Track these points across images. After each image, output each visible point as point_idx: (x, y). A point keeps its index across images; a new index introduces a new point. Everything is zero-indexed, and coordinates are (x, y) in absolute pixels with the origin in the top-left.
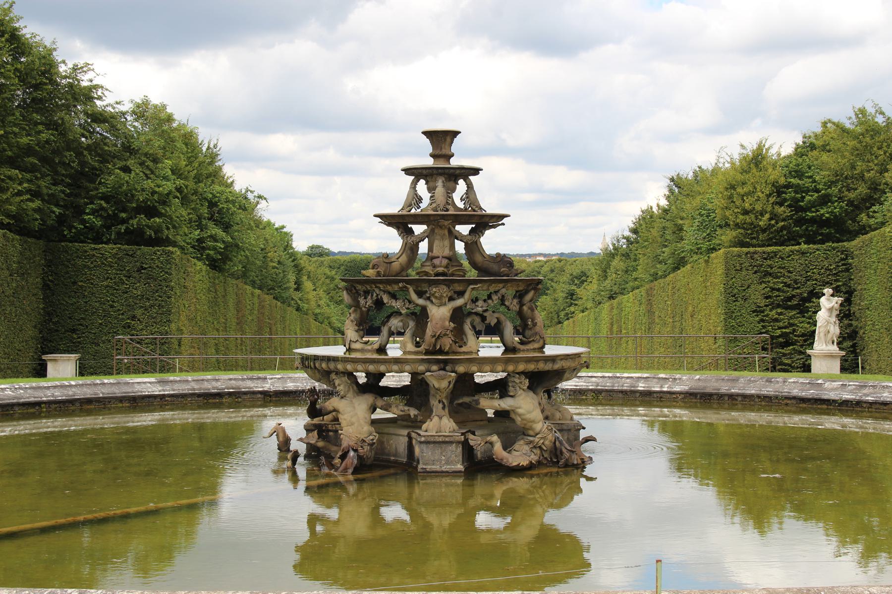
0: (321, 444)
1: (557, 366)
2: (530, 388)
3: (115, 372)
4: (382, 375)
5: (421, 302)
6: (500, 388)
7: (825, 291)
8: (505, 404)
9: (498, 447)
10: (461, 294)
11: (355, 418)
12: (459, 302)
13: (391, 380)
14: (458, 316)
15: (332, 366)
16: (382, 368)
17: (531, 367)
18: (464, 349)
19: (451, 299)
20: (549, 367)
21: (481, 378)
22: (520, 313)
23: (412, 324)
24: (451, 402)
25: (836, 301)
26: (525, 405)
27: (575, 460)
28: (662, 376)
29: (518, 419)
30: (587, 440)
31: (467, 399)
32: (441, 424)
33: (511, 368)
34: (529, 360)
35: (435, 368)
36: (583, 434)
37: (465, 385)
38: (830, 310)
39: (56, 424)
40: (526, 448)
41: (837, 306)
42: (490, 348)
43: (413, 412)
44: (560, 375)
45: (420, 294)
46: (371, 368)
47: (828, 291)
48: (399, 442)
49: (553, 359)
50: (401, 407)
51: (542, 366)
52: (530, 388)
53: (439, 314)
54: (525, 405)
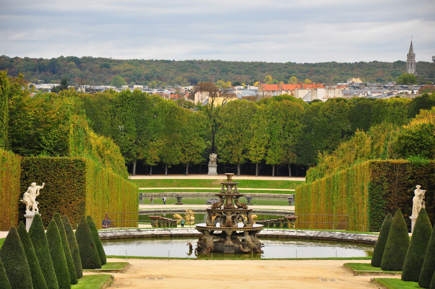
0: (201, 247)
5: (225, 215)
6: (242, 234)
7: (417, 186)
8: (243, 238)
9: (242, 247)
10: (234, 213)
11: (210, 241)
12: (233, 215)
14: (233, 218)
15: (205, 229)
17: (249, 230)
18: (234, 226)
19: (231, 214)
20: (253, 230)
21: (238, 232)
23: (222, 219)
24: (231, 237)
25: (423, 192)
26: (248, 238)
27: (258, 251)
31: (235, 237)
32: (229, 242)
33: (244, 230)
37: (234, 233)
38: (420, 196)
39: (288, 232)
40: (248, 248)
41: (423, 194)
43: (223, 239)
45: (224, 213)
46: (211, 230)
47: (418, 186)
48: (220, 246)
49: (254, 228)
53: (229, 217)
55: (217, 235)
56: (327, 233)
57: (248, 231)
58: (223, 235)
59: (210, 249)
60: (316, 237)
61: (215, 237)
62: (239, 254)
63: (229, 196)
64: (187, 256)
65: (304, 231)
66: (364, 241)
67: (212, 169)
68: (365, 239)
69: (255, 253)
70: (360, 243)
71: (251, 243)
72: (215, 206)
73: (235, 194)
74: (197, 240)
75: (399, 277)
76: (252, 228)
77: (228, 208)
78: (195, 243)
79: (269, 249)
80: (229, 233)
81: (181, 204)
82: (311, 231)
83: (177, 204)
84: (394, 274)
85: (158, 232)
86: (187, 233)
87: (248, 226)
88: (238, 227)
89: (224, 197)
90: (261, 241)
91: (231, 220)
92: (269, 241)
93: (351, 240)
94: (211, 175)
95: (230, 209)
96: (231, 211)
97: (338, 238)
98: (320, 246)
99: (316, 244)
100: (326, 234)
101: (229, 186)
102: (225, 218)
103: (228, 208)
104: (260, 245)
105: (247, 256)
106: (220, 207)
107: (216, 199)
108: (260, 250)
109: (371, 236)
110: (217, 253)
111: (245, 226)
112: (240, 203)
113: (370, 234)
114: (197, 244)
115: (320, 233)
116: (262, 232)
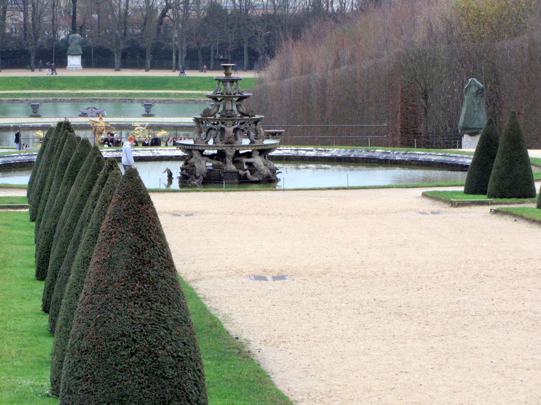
1: (268, 147)
2: (260, 155)
3: (117, 60)
4: (204, 150)
6: (249, 155)
13: (208, 152)
14: (235, 130)
15: (193, 148)
16: (204, 148)
17: (260, 148)
18: (237, 142)
19: (233, 125)
20: (266, 148)
22: (255, 129)
23: (219, 133)
26: (258, 160)
27: (273, 178)
28: (320, 149)
29: (255, 166)
30: (278, 173)
31: (239, 159)
33: (253, 148)
34: (258, 146)
35: (229, 148)
36: (277, 171)
37: (237, 154)
39: (304, 152)
42: (246, 142)
43: (221, 163)
44: (270, 150)
49: (267, 145)
50: (229, 165)
51: (263, 148)
52: (260, 155)
53: (230, 130)
54: (258, 160)
55: (211, 157)
56: (364, 151)
57: (259, 150)
58: (221, 156)
59: (201, 178)
60: (347, 158)
61: (209, 160)
62: (243, 182)
63: (227, 97)
64: (163, 187)
65: (327, 149)
66: (420, 161)
67: (74, 61)
68: (421, 158)
69: (269, 181)
70: (415, 165)
71: (263, 167)
72: (207, 113)
73: (237, 95)
74: (181, 164)
75: (534, 206)
76: (262, 146)
77: (228, 116)
78: (176, 168)
79: (287, 175)
80: (230, 153)
81: (39, 116)
82: (338, 149)
83: (32, 116)
84: (523, 202)
85: (108, 154)
86: (151, 155)
87: (258, 142)
88: (243, 144)
89: (219, 99)
90: (277, 165)
91: (232, 134)
92: (287, 166)
93: (400, 160)
94: (72, 70)
95: (230, 117)
96: (232, 120)
97: (381, 158)
98: (351, 170)
99: (347, 168)
100: (362, 152)
101: (228, 84)
102: (222, 130)
103: (228, 116)
104: (274, 171)
105: (255, 186)
106: (214, 115)
107: (95, 108)
108: (276, 177)
109: (430, 155)
110: (212, 180)
111: (252, 142)
112: (243, 109)
113: (428, 151)
114: (180, 171)
115: (339, 152)
116: (275, 153)
